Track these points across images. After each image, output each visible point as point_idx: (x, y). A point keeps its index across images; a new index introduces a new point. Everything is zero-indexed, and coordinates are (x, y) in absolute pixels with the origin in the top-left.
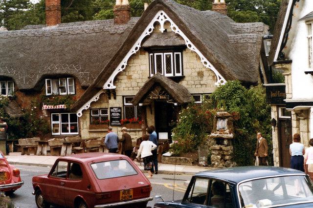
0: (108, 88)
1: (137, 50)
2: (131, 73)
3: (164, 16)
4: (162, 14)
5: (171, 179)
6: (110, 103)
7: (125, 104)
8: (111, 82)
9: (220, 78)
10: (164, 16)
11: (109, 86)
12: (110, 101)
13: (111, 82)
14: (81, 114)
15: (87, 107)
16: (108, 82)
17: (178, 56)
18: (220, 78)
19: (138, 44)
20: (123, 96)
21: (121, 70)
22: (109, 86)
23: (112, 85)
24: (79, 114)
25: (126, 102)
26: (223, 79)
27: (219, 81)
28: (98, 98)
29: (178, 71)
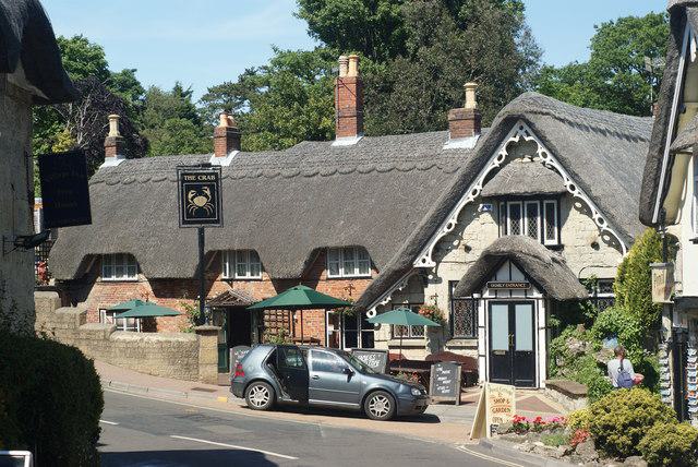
4: (521, 128)
11: (424, 261)
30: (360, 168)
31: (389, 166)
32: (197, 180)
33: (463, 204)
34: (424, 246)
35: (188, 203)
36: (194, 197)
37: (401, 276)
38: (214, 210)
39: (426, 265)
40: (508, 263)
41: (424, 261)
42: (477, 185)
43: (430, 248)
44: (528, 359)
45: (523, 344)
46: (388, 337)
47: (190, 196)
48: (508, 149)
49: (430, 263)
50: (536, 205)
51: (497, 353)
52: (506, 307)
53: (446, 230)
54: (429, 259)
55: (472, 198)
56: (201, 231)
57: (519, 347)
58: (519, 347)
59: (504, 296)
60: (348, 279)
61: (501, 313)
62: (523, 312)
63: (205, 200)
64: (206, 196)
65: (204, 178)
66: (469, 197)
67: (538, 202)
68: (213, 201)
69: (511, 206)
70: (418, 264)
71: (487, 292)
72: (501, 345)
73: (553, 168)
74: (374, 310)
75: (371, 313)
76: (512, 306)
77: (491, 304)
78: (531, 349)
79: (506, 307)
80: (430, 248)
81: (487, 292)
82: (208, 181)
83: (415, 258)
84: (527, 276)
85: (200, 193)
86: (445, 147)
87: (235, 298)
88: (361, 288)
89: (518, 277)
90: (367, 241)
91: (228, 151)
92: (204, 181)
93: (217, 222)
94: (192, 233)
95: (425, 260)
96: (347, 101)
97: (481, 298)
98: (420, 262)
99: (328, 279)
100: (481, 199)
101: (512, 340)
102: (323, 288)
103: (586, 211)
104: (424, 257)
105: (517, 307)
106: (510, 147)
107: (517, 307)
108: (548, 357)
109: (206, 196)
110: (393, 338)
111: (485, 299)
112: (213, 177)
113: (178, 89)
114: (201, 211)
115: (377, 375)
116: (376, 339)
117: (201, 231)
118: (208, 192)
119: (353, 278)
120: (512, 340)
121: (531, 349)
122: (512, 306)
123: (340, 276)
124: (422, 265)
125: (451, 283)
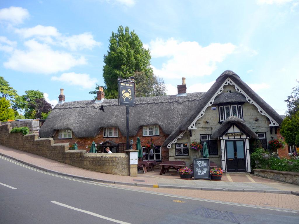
0: (191, 129)
1: (221, 92)
2: (179, 105)
3: (230, 82)
4: (228, 81)
5: (217, 158)
6: (191, 139)
7: (201, 140)
8: (193, 125)
9: (272, 122)
10: (230, 82)
11: (192, 127)
12: (191, 137)
13: (193, 125)
14: (170, 147)
15: (175, 142)
16: (191, 125)
17: (240, 107)
18: (272, 122)
19: (212, 100)
20: (200, 135)
21: (259, 110)
22: (192, 127)
23: (194, 127)
24: (169, 146)
25: (202, 139)
26: (274, 122)
27: (272, 123)
28: (183, 136)
29: (222, 119)
40: (233, 127)
44: (243, 161)
45: (240, 156)
50: (236, 107)
51: (230, 159)
52: (232, 143)
59: (231, 138)
64: (129, 93)
67: (236, 106)
69: (226, 107)
70: (190, 128)
72: (231, 156)
75: (169, 147)
82: (130, 87)
84: (240, 129)
85: (127, 91)
86: (52, 202)
89: (237, 130)
101: (236, 155)
102: (95, 167)
108: (251, 160)
109: (129, 93)
111: (224, 139)
113: (121, 30)
115: (255, 171)
116: (170, 156)
118: (130, 91)
120: (236, 155)
121: (243, 157)
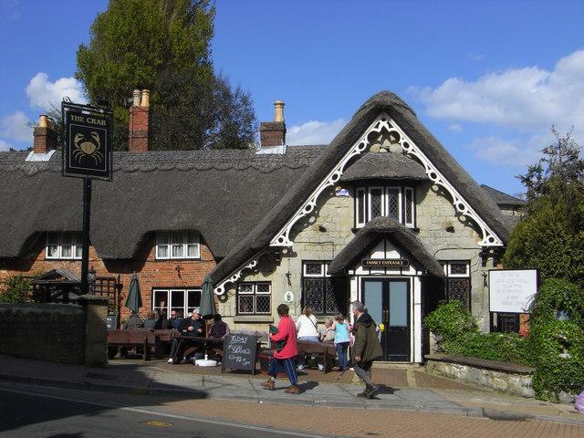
11: (281, 240)
30: (180, 166)
31: (208, 166)
32: (86, 124)
33: (325, 187)
34: (282, 226)
35: (73, 148)
36: (79, 143)
37: (256, 253)
38: (103, 160)
39: (283, 244)
40: (383, 242)
41: (281, 240)
42: (338, 171)
43: (288, 227)
45: (397, 320)
46: (234, 313)
47: (77, 140)
48: (369, 138)
49: (287, 242)
52: (380, 284)
53: (305, 212)
54: (286, 239)
55: (332, 183)
56: (88, 183)
57: (393, 323)
58: (393, 323)
60: (177, 260)
61: (375, 290)
62: (396, 290)
63: (94, 147)
65: (93, 121)
66: (329, 181)
68: (102, 150)
70: (275, 243)
71: (361, 268)
73: (414, 158)
74: (222, 286)
76: (386, 282)
77: (364, 280)
78: (405, 324)
79: (380, 284)
80: (288, 227)
81: (361, 268)
83: (273, 237)
85: (88, 138)
87: (59, 276)
88: (286, 266)
90: (200, 224)
91: (47, 150)
92: (93, 125)
93: (106, 174)
94: (77, 182)
95: (281, 240)
96: (139, 125)
97: (354, 275)
98: (277, 241)
99: (156, 261)
100: (342, 184)
103: (443, 192)
104: (282, 236)
105: (392, 284)
106: (373, 137)
107: (392, 284)
110: (237, 314)
112: (103, 123)
114: (88, 160)
117: (88, 183)
118: (97, 139)
119: (182, 260)
121: (405, 324)
122: (386, 282)
123: (71, 258)
124: (278, 244)
125: (313, 265)
